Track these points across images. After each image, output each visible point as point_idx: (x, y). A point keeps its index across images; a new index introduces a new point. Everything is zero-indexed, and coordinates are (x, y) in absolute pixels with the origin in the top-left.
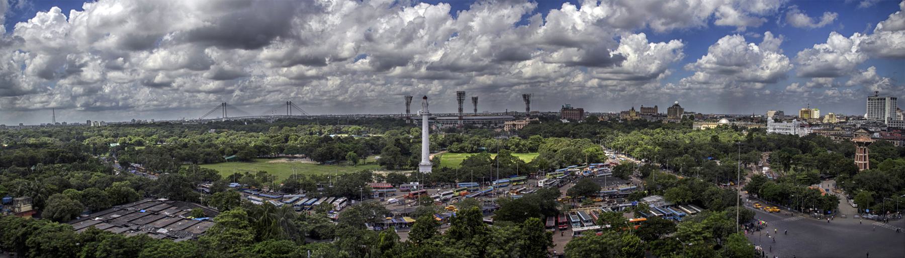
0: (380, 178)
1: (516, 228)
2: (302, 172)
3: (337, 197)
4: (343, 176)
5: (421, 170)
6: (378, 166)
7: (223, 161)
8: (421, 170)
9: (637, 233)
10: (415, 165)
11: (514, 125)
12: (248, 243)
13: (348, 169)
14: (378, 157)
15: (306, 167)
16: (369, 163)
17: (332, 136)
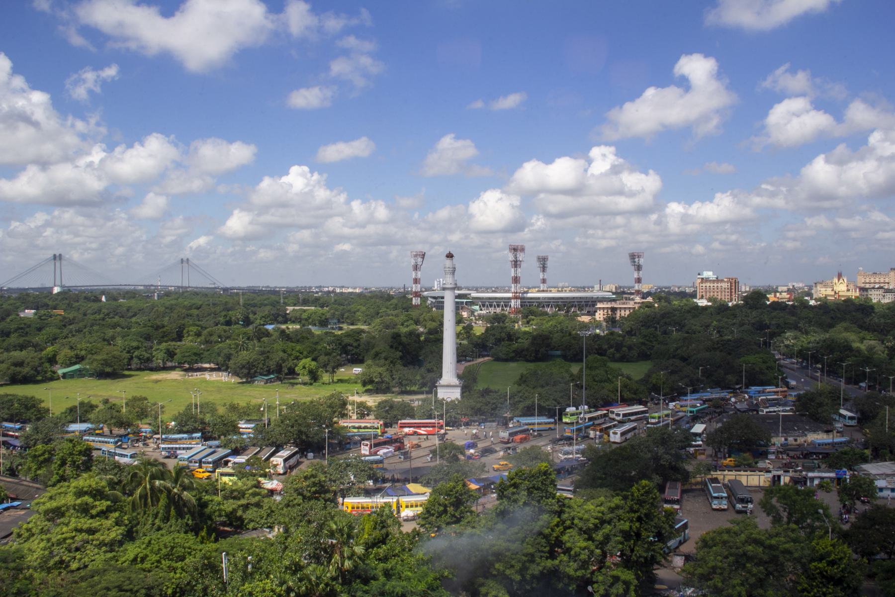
0: (363, 411)
1: (617, 500)
2: (211, 398)
3: (279, 448)
4: (291, 407)
5: (442, 394)
6: (359, 387)
7: (53, 378)
8: (442, 394)
9: (845, 537)
10: (431, 386)
11: (614, 310)
12: (112, 546)
13: (303, 394)
14: (357, 370)
15: (219, 388)
16: (341, 381)
17: (270, 327)
